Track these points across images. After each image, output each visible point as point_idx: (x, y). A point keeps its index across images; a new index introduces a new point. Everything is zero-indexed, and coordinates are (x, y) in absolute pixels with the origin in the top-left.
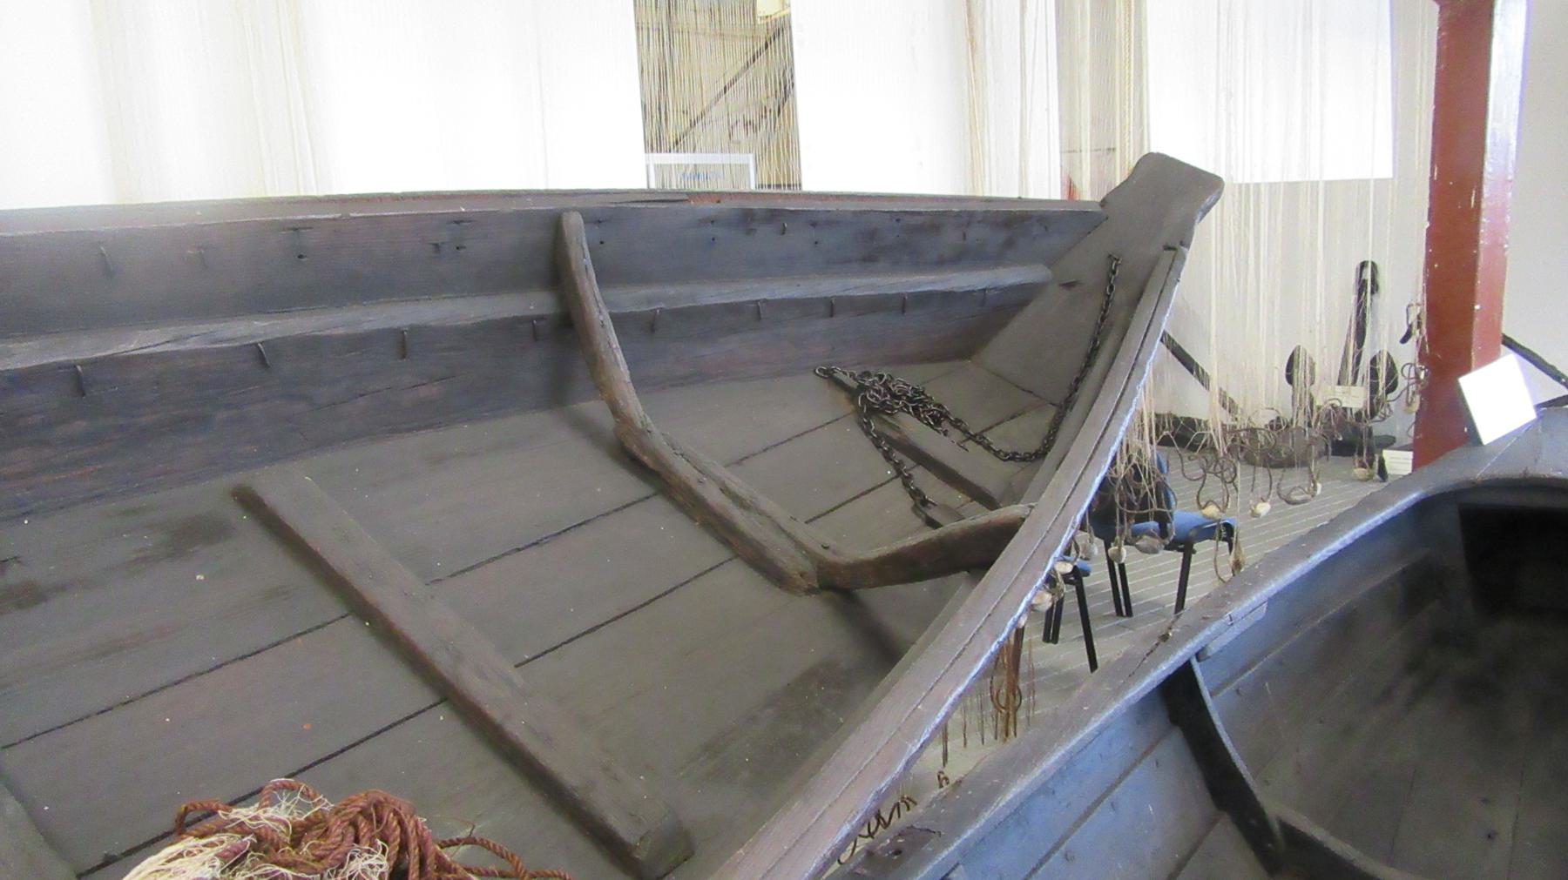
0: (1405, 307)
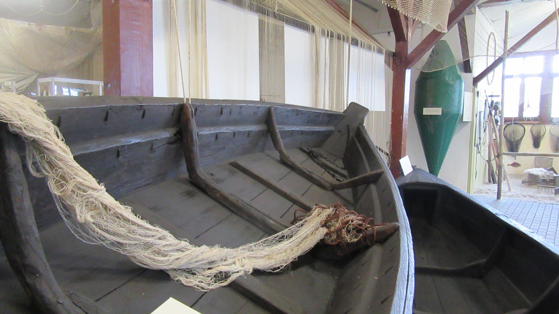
0: (386, 143)
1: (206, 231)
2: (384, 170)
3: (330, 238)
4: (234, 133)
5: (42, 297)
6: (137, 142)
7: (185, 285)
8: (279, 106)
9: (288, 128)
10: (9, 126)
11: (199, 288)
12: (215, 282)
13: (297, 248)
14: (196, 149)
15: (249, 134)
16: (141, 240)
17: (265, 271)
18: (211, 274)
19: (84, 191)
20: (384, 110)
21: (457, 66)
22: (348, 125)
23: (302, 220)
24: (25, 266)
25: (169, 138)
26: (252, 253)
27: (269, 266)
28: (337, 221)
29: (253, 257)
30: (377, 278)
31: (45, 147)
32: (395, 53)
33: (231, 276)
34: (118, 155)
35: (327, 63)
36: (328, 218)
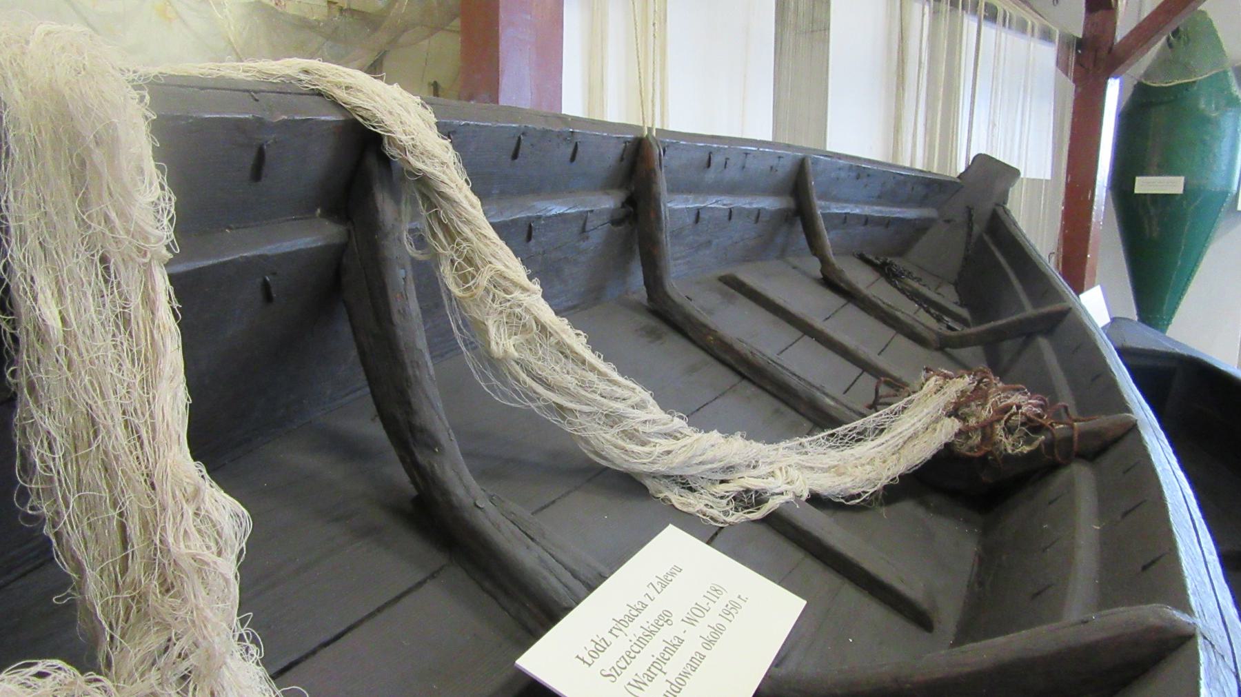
1: (698, 410)
2: (1071, 306)
3: (967, 441)
4: (731, 212)
5: (446, 493)
6: (561, 211)
7: (680, 509)
8: (822, 156)
9: (837, 208)
10: (386, 141)
11: (708, 518)
12: (736, 510)
13: (894, 457)
14: (666, 238)
15: (758, 217)
16: (602, 405)
17: (830, 500)
18: (727, 492)
19: (506, 291)
20: (1048, 177)
21: (1229, 74)
22: (968, 207)
23: (890, 404)
24: (412, 428)
25: (613, 210)
26: (804, 457)
27: (840, 489)
28: (983, 405)
29: (806, 467)
30: (1098, 528)
31: (441, 194)
32: (1081, 39)
33: (769, 499)
34: (529, 238)
35: (923, 61)
36: (962, 398)
